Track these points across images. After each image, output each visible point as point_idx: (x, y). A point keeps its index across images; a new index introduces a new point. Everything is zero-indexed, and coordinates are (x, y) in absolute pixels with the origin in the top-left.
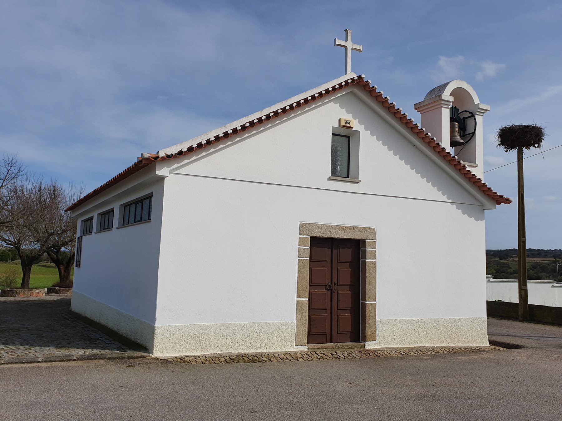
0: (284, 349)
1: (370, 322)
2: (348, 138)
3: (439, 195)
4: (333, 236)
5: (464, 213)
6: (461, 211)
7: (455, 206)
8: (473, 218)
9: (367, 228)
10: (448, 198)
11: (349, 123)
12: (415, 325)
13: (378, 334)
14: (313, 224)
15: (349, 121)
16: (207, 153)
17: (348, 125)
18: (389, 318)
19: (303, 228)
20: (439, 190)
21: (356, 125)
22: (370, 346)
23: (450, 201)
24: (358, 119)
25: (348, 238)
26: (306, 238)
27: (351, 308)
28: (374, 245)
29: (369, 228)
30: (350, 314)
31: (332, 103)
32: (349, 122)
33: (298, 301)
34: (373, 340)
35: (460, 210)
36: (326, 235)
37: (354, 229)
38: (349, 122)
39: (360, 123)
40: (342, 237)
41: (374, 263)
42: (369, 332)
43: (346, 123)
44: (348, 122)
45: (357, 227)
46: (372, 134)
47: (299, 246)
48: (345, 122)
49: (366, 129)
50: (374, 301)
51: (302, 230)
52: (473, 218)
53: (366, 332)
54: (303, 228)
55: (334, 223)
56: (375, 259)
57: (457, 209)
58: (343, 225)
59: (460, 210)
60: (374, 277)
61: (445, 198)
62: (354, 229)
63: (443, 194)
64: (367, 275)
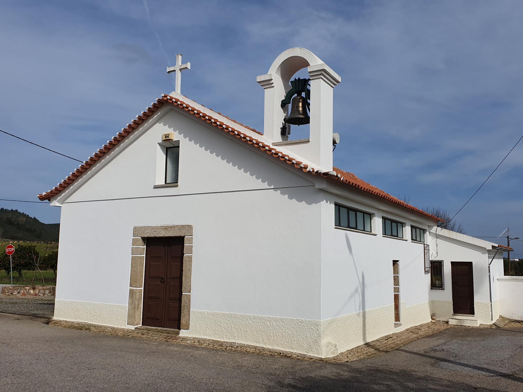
0: (119, 325)
1: (185, 312)
2: (168, 149)
3: (259, 184)
4: (157, 236)
5: (290, 198)
6: (280, 191)
7: (279, 192)
8: (304, 202)
9: (186, 225)
10: (269, 185)
11: (168, 137)
12: (228, 319)
13: (191, 323)
14: (142, 227)
15: (168, 134)
16: (69, 190)
17: (168, 138)
18: (202, 310)
19: (136, 231)
20: (258, 178)
21: (175, 136)
22: (183, 333)
23: (272, 187)
24: (178, 130)
25: (169, 236)
26: (138, 239)
27: (180, 277)
28: (191, 241)
29: (187, 225)
30: (179, 283)
31: (273, 190)
32: (168, 136)
33: (130, 290)
34: (186, 329)
35: (287, 196)
36: (152, 236)
37: (175, 228)
38: (168, 136)
39: (180, 133)
40: (165, 236)
41: (191, 258)
42: (183, 321)
43: (165, 137)
44: (167, 136)
45: (177, 226)
46: (190, 140)
47: (132, 245)
48: (165, 136)
49: (175, 130)
50: (189, 293)
51: (134, 233)
52: (304, 202)
53: (181, 321)
54: (136, 231)
55: (159, 224)
56: (192, 254)
57: (282, 195)
58: (166, 225)
59: (286, 195)
60: (190, 270)
61: (265, 185)
62: (175, 228)
63: (263, 181)
64: (184, 268)
